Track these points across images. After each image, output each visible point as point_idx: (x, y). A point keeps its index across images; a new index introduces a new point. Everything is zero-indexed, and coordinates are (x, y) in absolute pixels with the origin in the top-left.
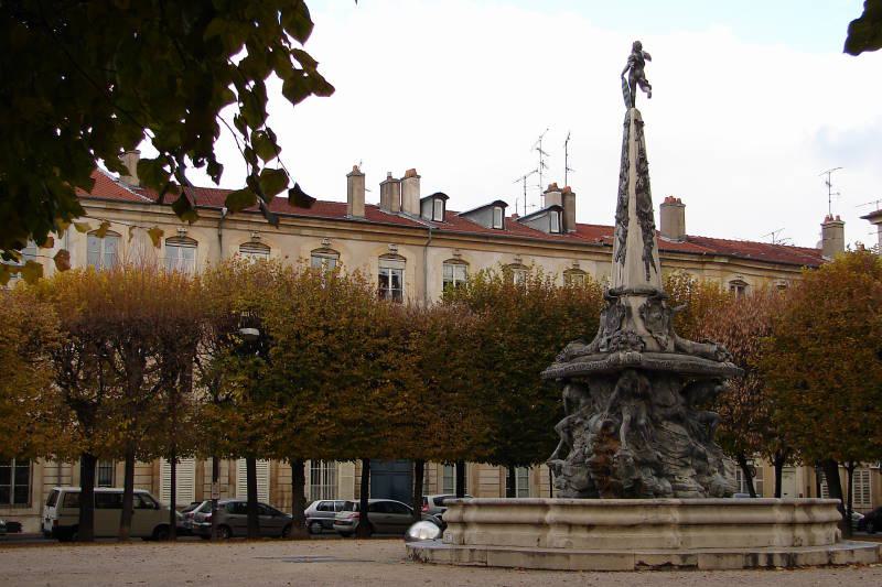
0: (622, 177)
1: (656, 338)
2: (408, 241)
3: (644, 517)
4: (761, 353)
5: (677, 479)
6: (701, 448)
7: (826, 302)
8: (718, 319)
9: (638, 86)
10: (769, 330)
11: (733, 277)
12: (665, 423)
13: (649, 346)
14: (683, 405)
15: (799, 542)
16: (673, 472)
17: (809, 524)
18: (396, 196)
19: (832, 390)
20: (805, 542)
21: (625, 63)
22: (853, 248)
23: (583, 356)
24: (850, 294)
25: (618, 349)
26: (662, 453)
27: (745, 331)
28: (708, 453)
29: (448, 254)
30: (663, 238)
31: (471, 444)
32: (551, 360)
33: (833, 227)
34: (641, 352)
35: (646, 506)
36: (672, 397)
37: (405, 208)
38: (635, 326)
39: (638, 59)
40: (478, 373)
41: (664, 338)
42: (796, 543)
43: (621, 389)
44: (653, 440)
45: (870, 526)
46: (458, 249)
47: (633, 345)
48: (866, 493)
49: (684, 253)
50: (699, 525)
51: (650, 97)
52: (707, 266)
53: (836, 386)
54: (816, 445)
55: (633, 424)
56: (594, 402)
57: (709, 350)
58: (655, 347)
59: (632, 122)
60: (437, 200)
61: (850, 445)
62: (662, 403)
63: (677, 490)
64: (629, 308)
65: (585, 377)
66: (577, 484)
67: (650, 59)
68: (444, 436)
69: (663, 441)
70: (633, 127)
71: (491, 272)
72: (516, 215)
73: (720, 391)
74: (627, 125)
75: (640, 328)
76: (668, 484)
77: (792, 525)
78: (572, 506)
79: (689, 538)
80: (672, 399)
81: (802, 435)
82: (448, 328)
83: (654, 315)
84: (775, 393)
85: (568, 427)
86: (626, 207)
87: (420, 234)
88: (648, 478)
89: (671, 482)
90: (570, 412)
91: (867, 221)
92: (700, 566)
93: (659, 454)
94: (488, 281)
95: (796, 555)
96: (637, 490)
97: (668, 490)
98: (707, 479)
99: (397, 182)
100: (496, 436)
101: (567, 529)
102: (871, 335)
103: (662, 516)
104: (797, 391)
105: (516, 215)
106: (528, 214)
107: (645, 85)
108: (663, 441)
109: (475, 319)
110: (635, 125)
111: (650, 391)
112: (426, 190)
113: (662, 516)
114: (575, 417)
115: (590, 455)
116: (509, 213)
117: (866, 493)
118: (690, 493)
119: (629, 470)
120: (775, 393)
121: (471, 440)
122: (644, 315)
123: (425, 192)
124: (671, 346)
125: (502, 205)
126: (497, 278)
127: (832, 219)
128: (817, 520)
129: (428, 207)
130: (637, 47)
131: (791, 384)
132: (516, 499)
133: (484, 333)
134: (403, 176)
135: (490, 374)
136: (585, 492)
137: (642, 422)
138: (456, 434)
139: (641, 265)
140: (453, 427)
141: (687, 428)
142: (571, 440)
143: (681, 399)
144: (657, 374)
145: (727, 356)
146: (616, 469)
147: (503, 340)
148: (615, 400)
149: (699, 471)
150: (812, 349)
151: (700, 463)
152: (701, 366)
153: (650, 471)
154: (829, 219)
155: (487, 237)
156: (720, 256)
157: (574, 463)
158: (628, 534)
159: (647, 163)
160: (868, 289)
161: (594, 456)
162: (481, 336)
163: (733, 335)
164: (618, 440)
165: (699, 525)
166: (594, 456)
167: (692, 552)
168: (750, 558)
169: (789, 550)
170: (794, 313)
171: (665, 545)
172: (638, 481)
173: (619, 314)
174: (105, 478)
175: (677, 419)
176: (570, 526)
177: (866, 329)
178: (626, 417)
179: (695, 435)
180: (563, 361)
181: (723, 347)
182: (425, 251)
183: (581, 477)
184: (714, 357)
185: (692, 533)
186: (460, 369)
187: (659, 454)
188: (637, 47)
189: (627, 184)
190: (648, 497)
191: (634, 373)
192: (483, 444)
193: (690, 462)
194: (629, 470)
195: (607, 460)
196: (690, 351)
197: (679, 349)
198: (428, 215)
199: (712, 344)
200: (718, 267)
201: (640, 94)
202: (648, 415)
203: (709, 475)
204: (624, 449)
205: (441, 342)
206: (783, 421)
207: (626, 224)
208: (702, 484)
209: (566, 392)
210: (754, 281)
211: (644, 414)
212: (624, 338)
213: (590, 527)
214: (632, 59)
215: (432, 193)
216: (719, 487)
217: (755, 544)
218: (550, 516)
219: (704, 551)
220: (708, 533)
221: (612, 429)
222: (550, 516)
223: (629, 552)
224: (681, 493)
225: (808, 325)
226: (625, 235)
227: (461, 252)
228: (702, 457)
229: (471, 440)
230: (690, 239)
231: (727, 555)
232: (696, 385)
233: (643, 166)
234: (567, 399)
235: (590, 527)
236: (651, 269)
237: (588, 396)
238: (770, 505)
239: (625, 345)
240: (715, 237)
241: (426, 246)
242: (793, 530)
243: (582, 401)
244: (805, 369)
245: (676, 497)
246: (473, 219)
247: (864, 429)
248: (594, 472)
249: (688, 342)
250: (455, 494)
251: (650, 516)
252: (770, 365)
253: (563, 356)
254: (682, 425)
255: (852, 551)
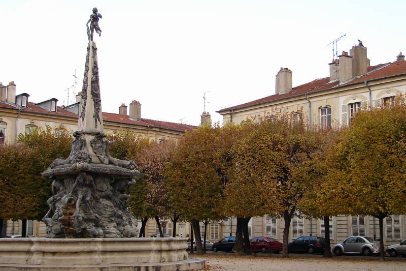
0: (85, 75)
1: (98, 157)
2: (7, 115)
3: (82, 248)
4: (165, 170)
5: (106, 228)
6: (120, 212)
7: (194, 146)
8: (147, 154)
9: (95, 30)
10: (169, 159)
11: (161, 137)
12: (101, 199)
13: (93, 161)
14: (111, 191)
15: (163, 260)
16: (104, 224)
17: (170, 250)
18: (4, 94)
19: (196, 187)
20: (167, 260)
21: (89, 18)
22: (213, 126)
23: (62, 165)
24: (205, 143)
25: (77, 161)
26: (99, 215)
27: (158, 159)
28: (123, 215)
29: (28, 122)
30: (130, 119)
31: (26, 210)
32: (47, 166)
33: (205, 117)
34: (89, 163)
35: (84, 242)
36: (106, 187)
37: (9, 100)
38: (88, 150)
39: (95, 17)
40: (30, 176)
41: (102, 157)
42: (162, 260)
43: (78, 181)
44: (94, 208)
45: (215, 249)
46: (32, 120)
47: (84, 159)
48: (216, 234)
49: (139, 126)
50: (112, 252)
51: (100, 36)
52: (150, 132)
53: (198, 185)
54: (188, 212)
55: (83, 199)
56: (66, 189)
57: (130, 167)
58: (98, 161)
59: (91, 48)
60: (24, 97)
61: (203, 212)
62: (100, 189)
63: (106, 233)
64: (85, 141)
65: (62, 175)
66: (55, 231)
67: (101, 17)
68: (12, 207)
69: (100, 209)
70: (91, 50)
71: (41, 129)
72: (64, 106)
73: (131, 184)
74: (88, 49)
75: (91, 151)
76: (101, 231)
77: (160, 251)
78: (45, 242)
79: (106, 259)
80: (105, 187)
81: (182, 207)
82: (16, 155)
83: (98, 145)
84: (171, 188)
85: (53, 201)
86: (86, 90)
87: (14, 111)
88: (91, 228)
89: (103, 230)
90: (56, 194)
91: (218, 113)
92: (337, 242)
93: (97, 215)
94: (39, 133)
95: (160, 267)
96: (84, 234)
97: (101, 234)
98: (122, 228)
99: (5, 87)
100: (39, 207)
101: (42, 254)
102: (214, 162)
103: (92, 247)
104: (180, 187)
105: (64, 106)
106: (69, 105)
107: (98, 29)
108: (100, 209)
109: (30, 151)
110: (93, 49)
111: (93, 183)
112: (18, 92)
113: (92, 247)
114: (57, 196)
115: (61, 216)
116: (59, 104)
117: (216, 234)
118: (112, 235)
119: (80, 223)
120: (171, 188)
121: (26, 209)
122: (93, 145)
123: (18, 93)
124: (106, 161)
125: (56, 100)
126: (44, 132)
127: (205, 113)
128: (173, 249)
129: (19, 100)
130: (95, 11)
131: (178, 184)
132: (177, 238)
133: (34, 157)
134: (8, 84)
135: (37, 177)
136: (60, 234)
137: (88, 199)
138: (18, 206)
139: (93, 120)
140: (17, 202)
141: (113, 203)
142: (55, 208)
143: (110, 188)
144: (97, 175)
145: (135, 166)
146: (73, 223)
147: (43, 161)
148: (75, 188)
149: (118, 224)
150: (188, 168)
151: (119, 220)
152: (116, 171)
153: (92, 224)
154: (204, 113)
155: (47, 115)
156: (155, 128)
157: (54, 220)
158: (73, 257)
159: (98, 69)
160: (213, 141)
161: (64, 216)
162: (33, 158)
163: (153, 161)
164: (75, 208)
165: (112, 252)
166: (64, 216)
167: (107, 266)
168: (136, 269)
169: (156, 265)
170: (181, 151)
171: (93, 262)
172: (85, 229)
173: (80, 144)
174: (40, 232)
175: (108, 197)
176: (44, 253)
177: (212, 159)
178: (80, 196)
179: (118, 206)
180: (52, 167)
181: (133, 162)
182: (16, 120)
183: (57, 227)
184: (128, 167)
185: (108, 256)
186: (21, 175)
187: (97, 215)
188: (95, 11)
189: (87, 79)
190: (90, 237)
191: (85, 174)
192: (32, 211)
193: (114, 220)
194: (80, 223)
195: (70, 218)
196: (117, 164)
197: (110, 162)
198: (19, 103)
199: (128, 160)
200: (154, 133)
201: (95, 34)
202: (92, 195)
203: (124, 226)
204: (78, 212)
205: (12, 161)
206: (174, 201)
207: (86, 99)
208: (119, 230)
209: (53, 183)
210: (167, 137)
211: (89, 195)
212: (80, 156)
213: (54, 253)
214: (92, 16)
215: (21, 93)
216: (128, 232)
217: (140, 262)
218: (34, 248)
219: (113, 265)
220: (117, 257)
221: (73, 202)
222: (34, 248)
223: (72, 267)
224: (107, 235)
225: (187, 157)
226: (85, 105)
227: (34, 121)
228: (120, 217)
229: (26, 209)
230: (143, 120)
231: (124, 267)
232: (118, 180)
233: (95, 70)
234: (54, 187)
235: (54, 253)
236: (98, 122)
237: (64, 185)
238: (150, 241)
239: (80, 159)
240: (154, 119)
241: (17, 117)
242: (161, 254)
243: (61, 188)
244: (184, 177)
245: (105, 237)
246: (42, 107)
247: (209, 205)
248: (63, 225)
249: (116, 159)
250: (21, 235)
251: (86, 247)
252: (169, 175)
253: (52, 165)
254: (111, 201)
255: (189, 264)
